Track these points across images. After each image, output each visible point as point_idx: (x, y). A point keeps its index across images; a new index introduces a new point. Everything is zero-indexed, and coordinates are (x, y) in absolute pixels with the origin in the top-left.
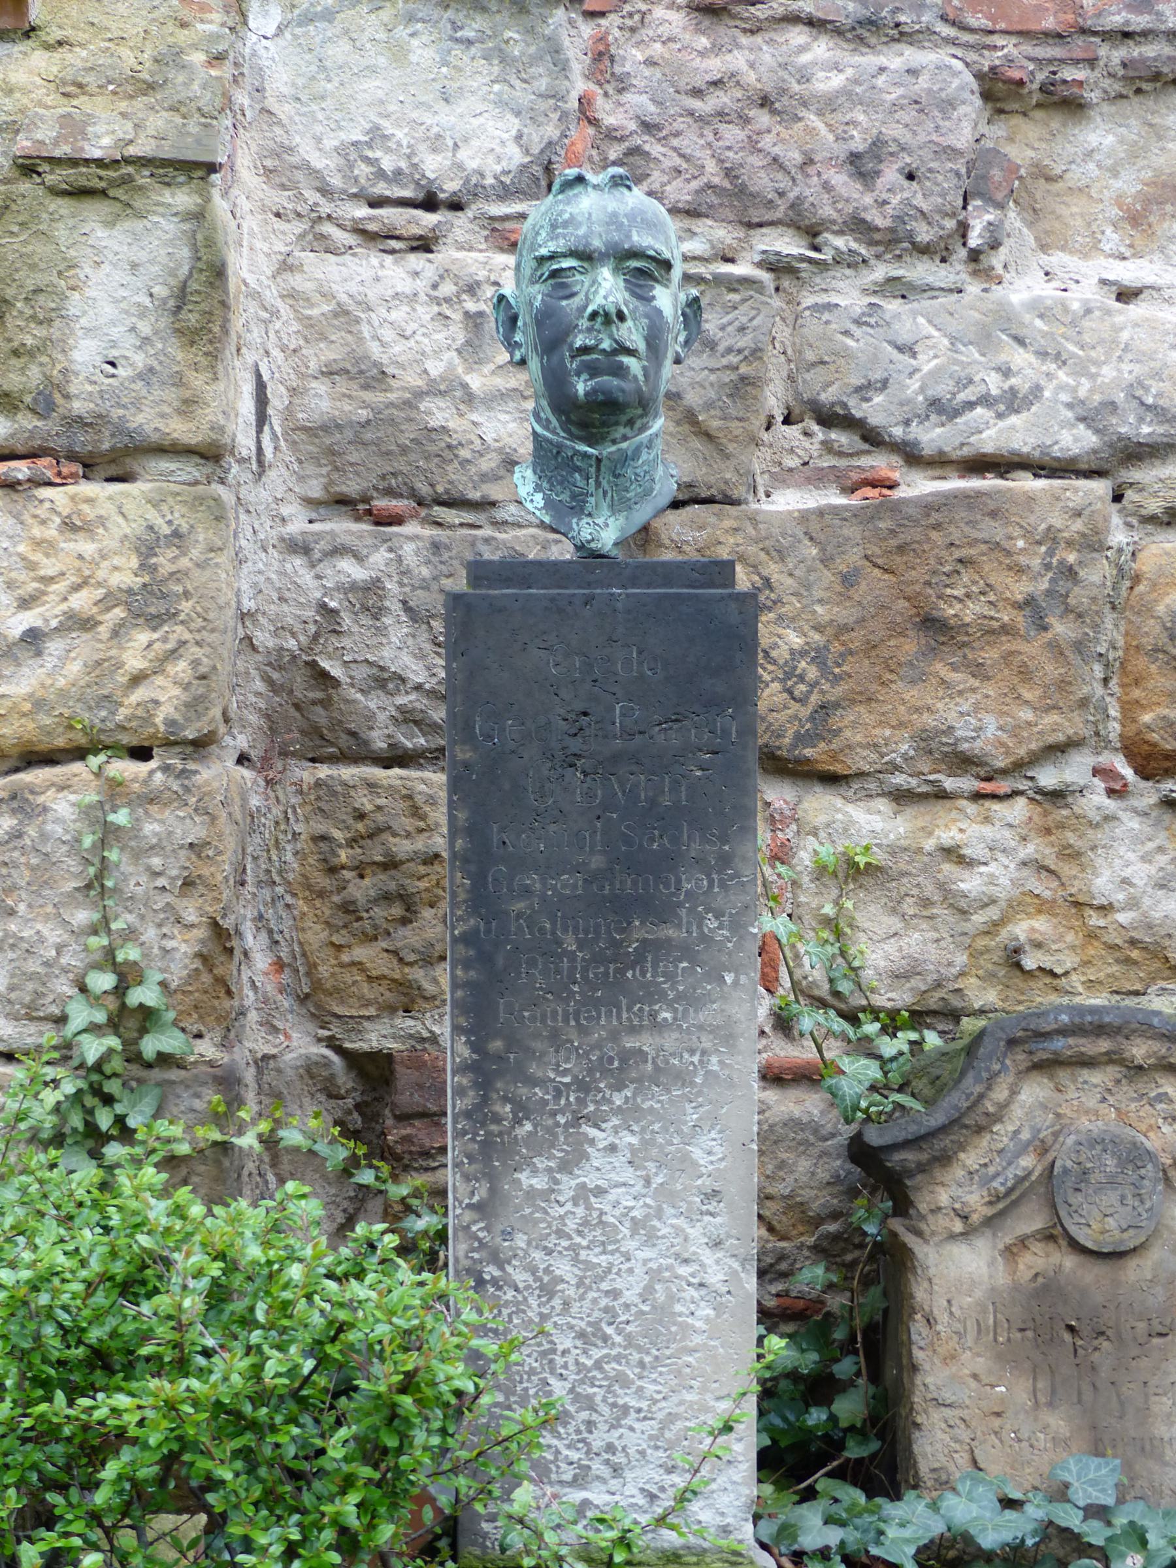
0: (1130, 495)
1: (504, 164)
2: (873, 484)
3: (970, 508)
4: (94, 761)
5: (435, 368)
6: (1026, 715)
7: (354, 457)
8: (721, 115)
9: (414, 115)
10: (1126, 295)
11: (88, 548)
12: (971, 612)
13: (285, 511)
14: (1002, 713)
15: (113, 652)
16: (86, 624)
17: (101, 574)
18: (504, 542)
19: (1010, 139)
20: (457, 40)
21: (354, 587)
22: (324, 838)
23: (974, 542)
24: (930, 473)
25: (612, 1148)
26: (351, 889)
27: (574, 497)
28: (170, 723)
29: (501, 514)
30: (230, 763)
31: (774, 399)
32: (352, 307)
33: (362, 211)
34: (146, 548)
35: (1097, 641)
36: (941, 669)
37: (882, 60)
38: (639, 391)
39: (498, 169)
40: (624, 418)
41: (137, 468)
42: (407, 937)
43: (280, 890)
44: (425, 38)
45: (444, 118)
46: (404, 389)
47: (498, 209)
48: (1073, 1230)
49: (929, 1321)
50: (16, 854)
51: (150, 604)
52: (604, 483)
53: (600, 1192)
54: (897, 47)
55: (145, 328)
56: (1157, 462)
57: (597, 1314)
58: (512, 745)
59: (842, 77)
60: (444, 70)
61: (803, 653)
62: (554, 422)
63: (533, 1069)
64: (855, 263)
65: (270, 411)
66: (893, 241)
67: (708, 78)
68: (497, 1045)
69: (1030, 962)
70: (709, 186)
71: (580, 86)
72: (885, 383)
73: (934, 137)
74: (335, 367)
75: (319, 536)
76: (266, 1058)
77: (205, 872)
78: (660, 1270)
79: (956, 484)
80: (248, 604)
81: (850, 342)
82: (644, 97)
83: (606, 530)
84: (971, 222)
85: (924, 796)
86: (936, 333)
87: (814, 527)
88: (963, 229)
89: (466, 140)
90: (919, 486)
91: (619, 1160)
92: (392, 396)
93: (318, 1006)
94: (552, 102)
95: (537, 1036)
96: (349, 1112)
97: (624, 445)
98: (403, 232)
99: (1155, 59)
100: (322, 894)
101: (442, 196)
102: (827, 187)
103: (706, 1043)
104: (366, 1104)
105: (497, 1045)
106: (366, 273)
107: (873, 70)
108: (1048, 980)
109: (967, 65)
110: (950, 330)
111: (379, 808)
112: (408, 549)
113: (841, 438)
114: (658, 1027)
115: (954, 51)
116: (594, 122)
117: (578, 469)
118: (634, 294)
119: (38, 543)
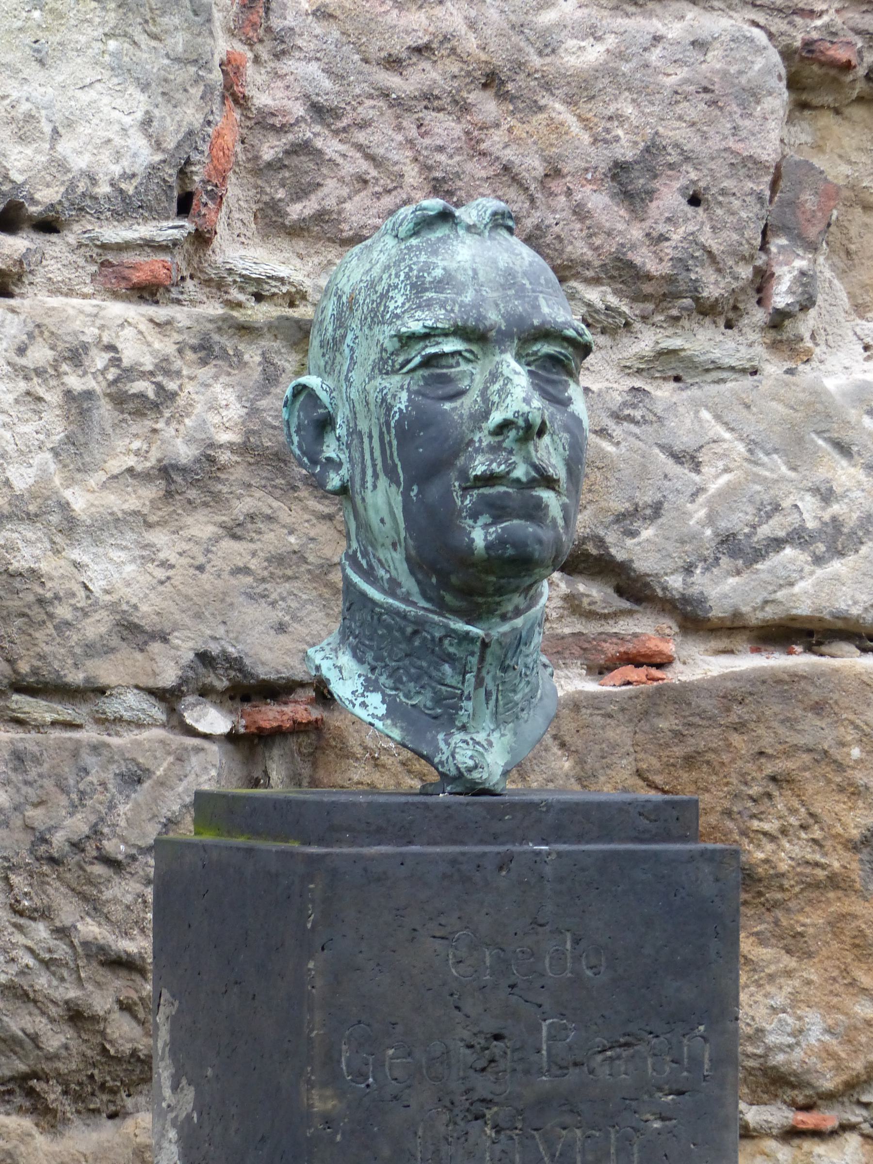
1: (125, 163)
3: (785, 697)
8: (429, 98)
12: (787, 855)
14: (831, 1008)
18: (121, 751)
19: (818, 148)
23: (792, 751)
24: (714, 644)
27: (438, 700)
29: (113, 707)
37: (656, 25)
39: (116, 170)
45: (37, 90)
47: (114, 233)
52: (488, 680)
58: (393, 1088)
59: (600, 48)
60: (36, 14)
66: (668, 296)
67: (410, 41)
71: (222, 45)
72: (657, 509)
73: (731, 143)
79: (748, 662)
81: (607, 447)
82: (313, 68)
84: (778, 270)
86: (727, 435)
87: (568, 726)
88: (762, 281)
89: (70, 124)
90: (701, 665)
94: (193, 69)
97: (519, 622)
102: (580, 212)
107: (646, 39)
109: (771, 36)
110: (748, 430)
116: (241, 101)
117: (450, 659)
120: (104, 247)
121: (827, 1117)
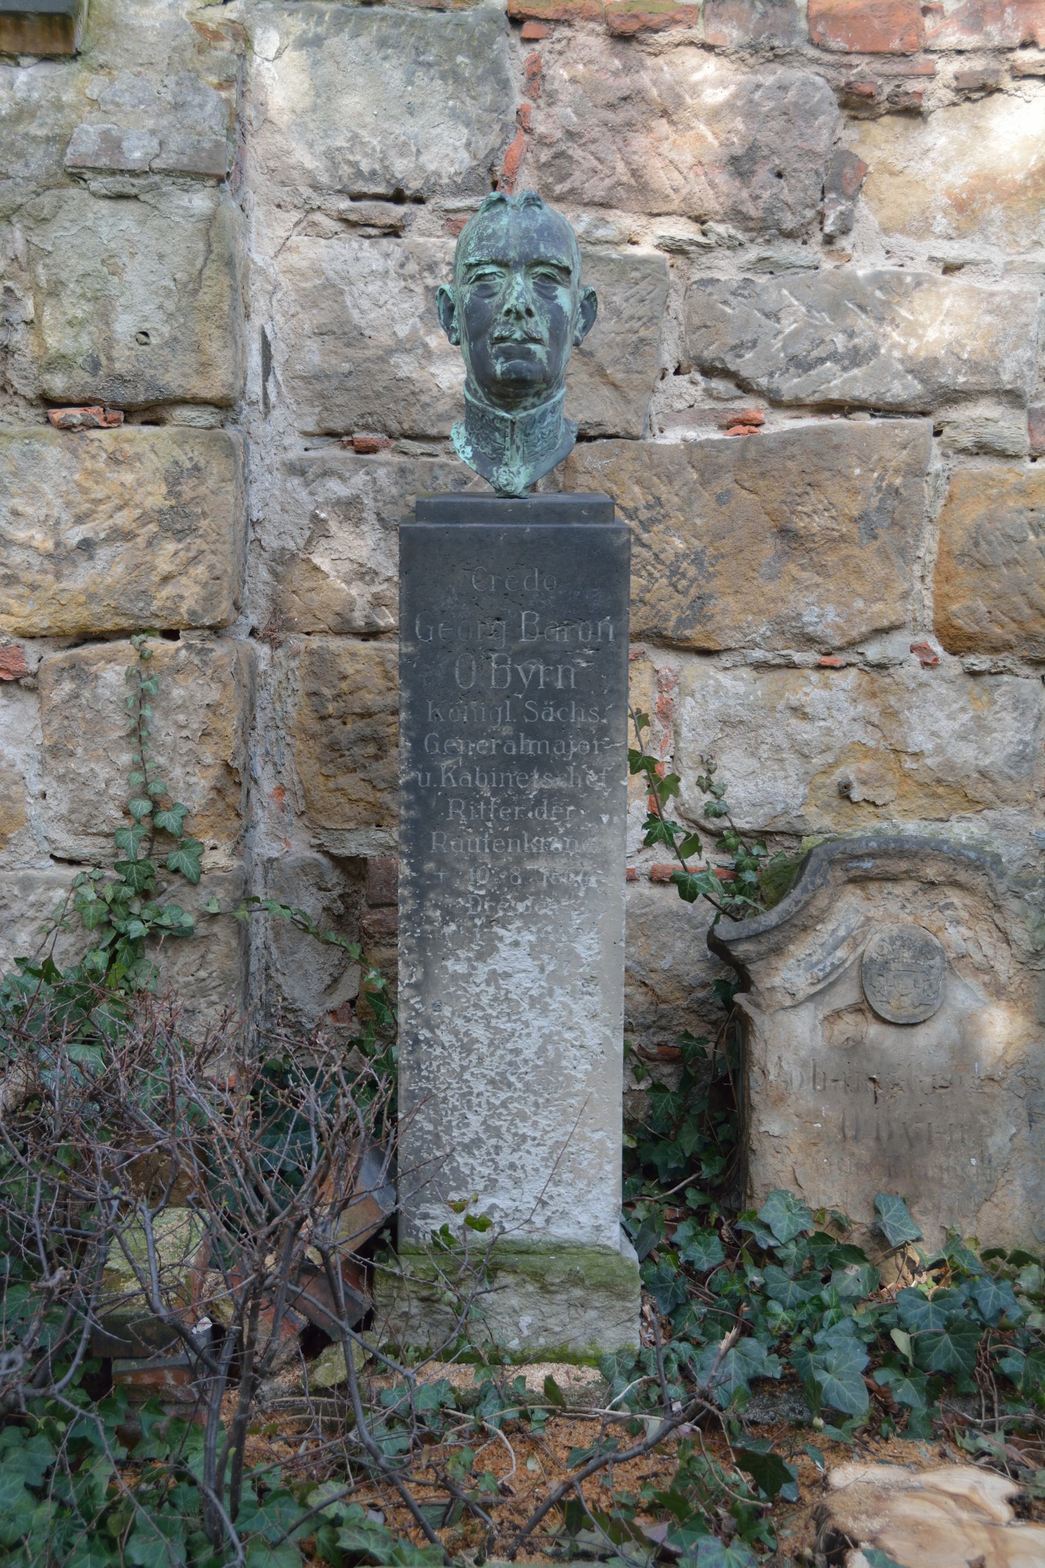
0: (947, 430)
2: (744, 423)
4: (137, 639)
5: (403, 331)
6: (859, 604)
7: (339, 400)
9: (386, 125)
10: (950, 269)
11: (129, 478)
12: (817, 523)
13: (287, 441)
15: (148, 558)
16: (128, 536)
17: (138, 498)
20: (420, 63)
21: (338, 502)
22: (315, 694)
24: (789, 413)
25: (516, 944)
26: (336, 731)
27: (494, 450)
28: (192, 613)
30: (243, 637)
31: (669, 355)
32: (338, 281)
33: (345, 204)
34: (173, 480)
35: (917, 548)
36: (793, 568)
37: (760, 78)
38: (543, 371)
40: (532, 391)
41: (166, 416)
42: (379, 770)
43: (282, 733)
44: (394, 61)
45: (409, 128)
46: (377, 347)
48: (876, 1006)
49: (764, 1073)
50: (74, 711)
51: (176, 521)
53: (507, 975)
54: (772, 66)
55: (170, 306)
56: (970, 405)
57: (503, 1067)
61: (686, 556)
62: (480, 393)
63: (457, 884)
64: (735, 246)
65: (274, 364)
67: (619, 94)
68: (429, 866)
69: (856, 795)
70: (620, 184)
72: (754, 343)
73: (799, 142)
74: (324, 330)
75: (312, 462)
76: (271, 860)
77: (219, 725)
78: (551, 1035)
79: (809, 422)
80: (256, 515)
83: (516, 475)
85: (778, 666)
88: (821, 217)
90: (781, 424)
91: (521, 952)
92: (369, 353)
93: (311, 821)
95: (459, 860)
96: (334, 901)
97: (533, 411)
98: (378, 222)
99: (982, 72)
100: (313, 736)
101: (408, 193)
103: (587, 868)
104: (349, 895)
105: (429, 866)
106: (348, 255)
108: (872, 809)
111: (358, 671)
112: (381, 473)
113: (719, 385)
114: (553, 854)
115: (821, 70)
116: (528, 131)
117: (498, 430)
118: (540, 294)
119: (89, 473)
120: (447, 211)
121: (839, 659)
